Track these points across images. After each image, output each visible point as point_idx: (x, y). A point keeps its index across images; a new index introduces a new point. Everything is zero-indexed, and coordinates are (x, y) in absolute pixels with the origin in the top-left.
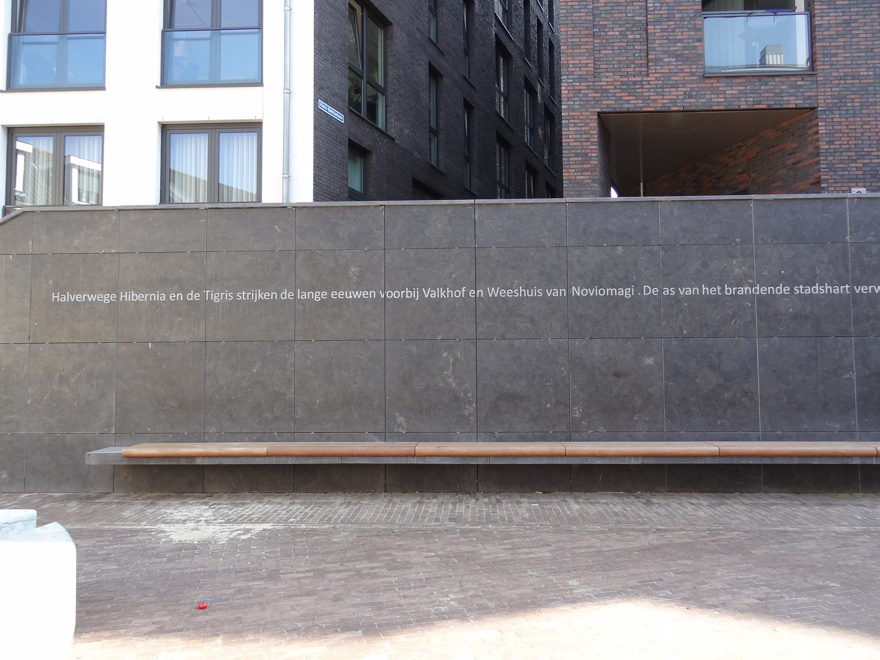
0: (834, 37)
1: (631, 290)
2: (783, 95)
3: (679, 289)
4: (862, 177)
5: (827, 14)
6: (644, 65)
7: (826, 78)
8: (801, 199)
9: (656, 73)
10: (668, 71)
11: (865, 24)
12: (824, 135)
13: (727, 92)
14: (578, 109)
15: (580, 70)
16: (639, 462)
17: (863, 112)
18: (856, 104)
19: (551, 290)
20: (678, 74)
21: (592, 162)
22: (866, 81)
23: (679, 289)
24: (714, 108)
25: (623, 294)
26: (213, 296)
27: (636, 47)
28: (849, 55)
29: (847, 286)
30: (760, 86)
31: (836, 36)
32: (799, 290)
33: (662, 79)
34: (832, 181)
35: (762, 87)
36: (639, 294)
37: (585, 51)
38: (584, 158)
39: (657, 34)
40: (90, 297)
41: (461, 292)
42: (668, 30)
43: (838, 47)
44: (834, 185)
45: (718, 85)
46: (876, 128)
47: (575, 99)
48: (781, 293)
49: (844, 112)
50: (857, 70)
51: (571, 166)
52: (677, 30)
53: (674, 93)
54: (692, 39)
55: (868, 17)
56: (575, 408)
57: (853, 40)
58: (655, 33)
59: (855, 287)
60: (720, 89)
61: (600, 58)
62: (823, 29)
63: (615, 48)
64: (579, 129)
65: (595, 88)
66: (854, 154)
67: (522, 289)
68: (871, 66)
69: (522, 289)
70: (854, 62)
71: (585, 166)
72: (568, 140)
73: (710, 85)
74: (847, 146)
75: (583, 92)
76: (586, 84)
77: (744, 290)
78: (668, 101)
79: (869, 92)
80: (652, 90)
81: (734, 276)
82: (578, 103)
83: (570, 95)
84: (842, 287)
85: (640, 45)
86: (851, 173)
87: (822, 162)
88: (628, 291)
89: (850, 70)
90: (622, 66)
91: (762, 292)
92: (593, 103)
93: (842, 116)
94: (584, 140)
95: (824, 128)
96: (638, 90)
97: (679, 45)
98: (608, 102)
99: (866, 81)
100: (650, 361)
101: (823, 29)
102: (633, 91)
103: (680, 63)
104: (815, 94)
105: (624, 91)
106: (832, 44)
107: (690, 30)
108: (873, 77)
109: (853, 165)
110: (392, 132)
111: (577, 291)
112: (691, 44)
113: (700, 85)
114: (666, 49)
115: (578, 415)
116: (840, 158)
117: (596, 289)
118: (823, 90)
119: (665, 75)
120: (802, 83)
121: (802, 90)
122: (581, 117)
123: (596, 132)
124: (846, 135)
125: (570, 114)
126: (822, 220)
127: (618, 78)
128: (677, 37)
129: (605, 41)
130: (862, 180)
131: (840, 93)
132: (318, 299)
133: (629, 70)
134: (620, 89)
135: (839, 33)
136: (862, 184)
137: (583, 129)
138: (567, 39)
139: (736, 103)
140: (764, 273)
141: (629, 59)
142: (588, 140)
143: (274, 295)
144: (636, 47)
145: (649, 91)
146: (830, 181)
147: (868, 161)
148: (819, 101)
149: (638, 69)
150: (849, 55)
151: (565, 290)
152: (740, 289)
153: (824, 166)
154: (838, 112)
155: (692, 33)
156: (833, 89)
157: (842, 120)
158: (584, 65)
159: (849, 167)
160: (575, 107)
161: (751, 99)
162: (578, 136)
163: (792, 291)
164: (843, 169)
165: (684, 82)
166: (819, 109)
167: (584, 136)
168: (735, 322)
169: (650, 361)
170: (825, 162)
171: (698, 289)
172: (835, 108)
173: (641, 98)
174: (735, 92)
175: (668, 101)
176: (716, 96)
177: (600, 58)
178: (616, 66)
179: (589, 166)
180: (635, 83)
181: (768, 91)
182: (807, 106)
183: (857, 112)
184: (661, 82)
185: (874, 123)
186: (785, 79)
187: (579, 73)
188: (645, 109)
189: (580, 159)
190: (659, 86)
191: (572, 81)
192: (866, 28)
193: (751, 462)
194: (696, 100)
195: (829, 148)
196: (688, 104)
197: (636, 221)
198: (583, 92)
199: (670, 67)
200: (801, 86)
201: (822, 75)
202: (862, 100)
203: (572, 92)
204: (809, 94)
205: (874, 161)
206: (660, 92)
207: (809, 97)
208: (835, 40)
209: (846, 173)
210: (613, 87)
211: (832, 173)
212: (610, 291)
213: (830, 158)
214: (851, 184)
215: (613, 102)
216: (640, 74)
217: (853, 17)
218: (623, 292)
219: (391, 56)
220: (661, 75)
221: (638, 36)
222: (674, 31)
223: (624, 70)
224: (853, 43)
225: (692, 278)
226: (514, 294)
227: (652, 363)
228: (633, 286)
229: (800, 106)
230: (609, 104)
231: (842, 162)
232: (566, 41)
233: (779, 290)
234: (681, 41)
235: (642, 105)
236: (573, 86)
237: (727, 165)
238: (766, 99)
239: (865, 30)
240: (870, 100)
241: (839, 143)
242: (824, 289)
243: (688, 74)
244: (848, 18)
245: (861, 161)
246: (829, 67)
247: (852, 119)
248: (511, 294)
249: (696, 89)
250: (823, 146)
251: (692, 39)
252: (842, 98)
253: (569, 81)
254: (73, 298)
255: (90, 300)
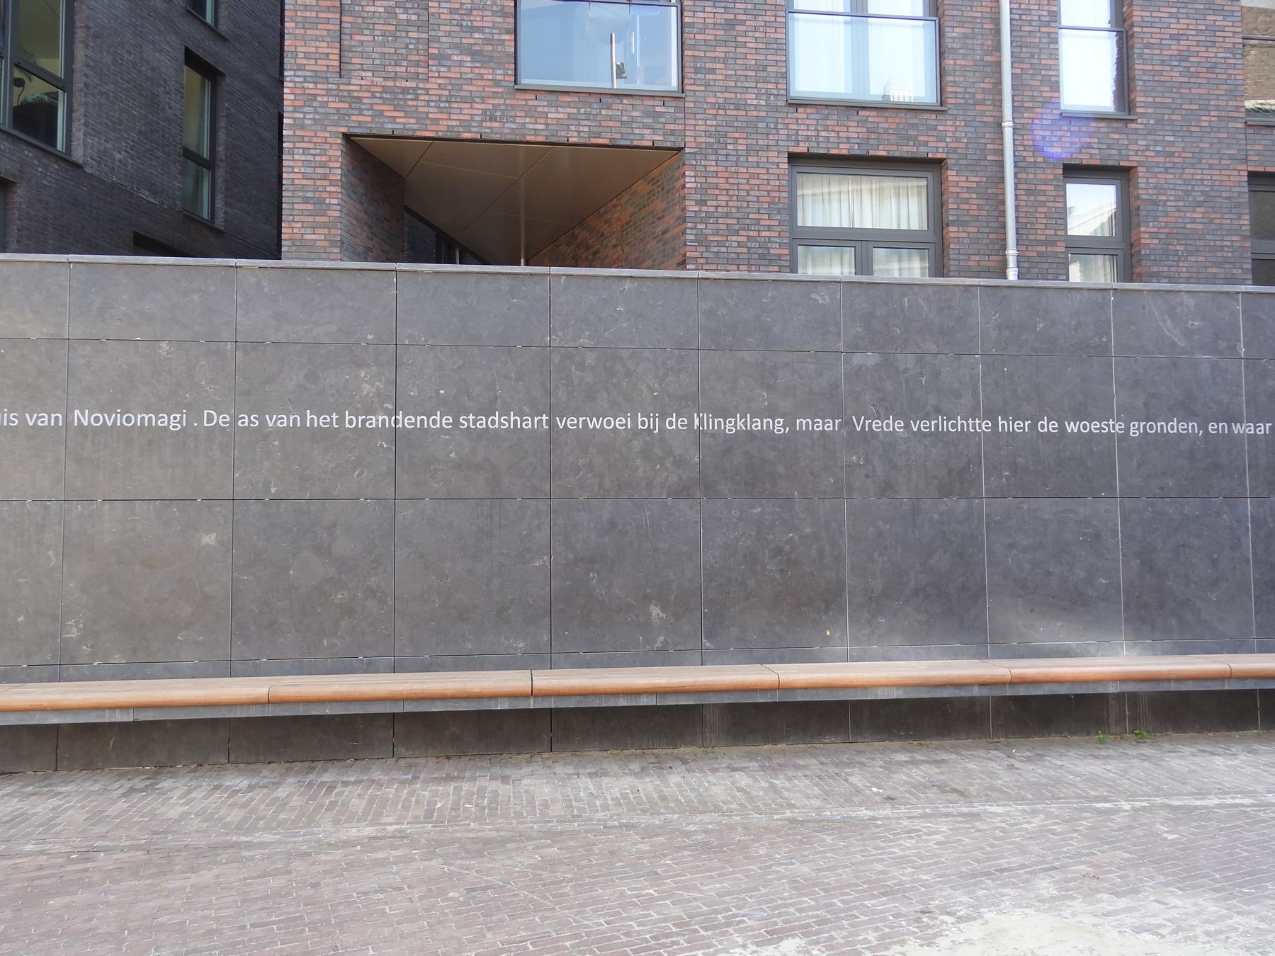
1: (181, 418)
2: (634, 125)
3: (267, 416)
5: (701, 9)
6: (422, 64)
8: (477, 273)
9: (439, 77)
10: (458, 76)
11: (756, 29)
12: (694, 191)
13: (549, 115)
14: (311, 125)
15: (316, 64)
16: (129, 717)
19: (36, 415)
20: (474, 82)
21: (330, 213)
22: (755, 113)
23: (267, 416)
24: (528, 138)
25: (166, 424)
27: (410, 34)
28: (733, 72)
29: (545, 418)
30: (600, 109)
31: (713, 43)
32: (467, 421)
33: (450, 87)
34: (703, 261)
35: (604, 112)
36: (196, 424)
37: (325, 33)
38: (318, 207)
39: (443, 16)
42: (461, 12)
45: (536, 103)
46: (768, 184)
47: (306, 109)
48: (438, 426)
49: (724, 158)
50: (743, 96)
51: (296, 218)
52: (474, 12)
53: (467, 111)
54: (498, 28)
55: (760, 18)
56: (70, 623)
57: (739, 50)
58: (439, 14)
59: (27, 415)
60: (540, 109)
61: (352, 46)
62: (695, 30)
63: (377, 33)
64: (310, 158)
65: (341, 94)
66: (735, 221)
68: (763, 91)
70: (739, 84)
71: (318, 219)
72: (291, 176)
73: (524, 103)
74: (725, 209)
75: (319, 99)
76: (325, 86)
77: (377, 420)
78: (458, 123)
80: (432, 104)
81: (360, 396)
82: (311, 116)
83: (297, 103)
84: (536, 419)
85: (418, 32)
86: (730, 250)
87: (688, 231)
88: (175, 418)
89: (733, 96)
90: (387, 63)
91: (406, 425)
92: (336, 117)
93: (719, 163)
94: (319, 176)
95: (693, 179)
96: (410, 103)
97: (476, 35)
98: (361, 118)
99: (755, 113)
100: (209, 539)
101: (695, 30)
102: (402, 103)
103: (478, 65)
104: (681, 127)
105: (387, 102)
106: (708, 54)
107: (494, 13)
108: (765, 108)
109: (734, 238)
110: (78, 155)
111: (82, 417)
112: (496, 37)
113: (508, 102)
114: (457, 40)
115: (74, 634)
116: (715, 226)
117: (119, 415)
119: (453, 81)
120: (663, 109)
122: (315, 140)
123: (338, 165)
124: (725, 192)
125: (297, 134)
126: (508, 309)
127: (379, 81)
128: (475, 24)
129: (360, 20)
130: (746, 262)
131: (718, 128)
132: (1135, 433)
133: (398, 69)
134: (380, 98)
135: (718, 38)
137: (318, 158)
138: (296, 11)
139: (563, 134)
140: (412, 393)
141: (398, 52)
142: (324, 177)
144: (410, 34)
145: (428, 106)
147: (755, 234)
149: (412, 70)
151: (60, 416)
152: (371, 419)
153: (692, 237)
154: (713, 157)
155: (498, 20)
157: (720, 169)
158: (322, 56)
160: (306, 122)
161: (586, 129)
162: (309, 170)
163: (456, 423)
165: (483, 95)
166: (687, 150)
167: (318, 170)
168: (359, 475)
169: (209, 539)
170: (694, 232)
171: (298, 418)
172: (710, 151)
173: (414, 115)
174: (561, 116)
175: (458, 123)
176: (532, 120)
177: (352, 46)
178: (377, 62)
179: (325, 219)
180: (405, 91)
181: (611, 118)
182: (669, 145)
183: (742, 159)
184: (446, 93)
185: (766, 177)
186: (637, 102)
187: (314, 68)
188: (419, 134)
189: (310, 207)
190: (444, 99)
191: (302, 79)
192: (757, 34)
193: (328, 712)
194: (501, 125)
195: (700, 211)
196: (489, 131)
197: (196, 299)
198: (319, 99)
199: (463, 70)
200: (661, 114)
201: (692, 99)
203: (301, 97)
204: (672, 127)
205: (764, 234)
206: (445, 107)
207: (673, 132)
208: (712, 49)
209: (723, 249)
210: (368, 95)
211: (703, 249)
212: (143, 419)
213: (699, 226)
215: (369, 119)
216: (416, 77)
217: (739, 17)
218: (166, 420)
219: (81, 27)
220: (447, 81)
221: (414, 17)
222: (470, 14)
223: (390, 69)
224: (738, 56)
225: (290, 399)
226: (1101, 428)
227: (214, 543)
228: (185, 411)
229: (660, 145)
230: (361, 122)
231: (717, 232)
232: (294, 14)
233: (435, 422)
234: (480, 30)
235: (416, 126)
236: (303, 87)
237: (602, 234)
238: (608, 130)
240: (761, 142)
241: (714, 203)
242: (509, 421)
243: (491, 83)
244: (732, 17)
246: (703, 88)
247: (733, 169)
249: (503, 107)
250: (692, 207)
251: (498, 28)
252: (721, 137)
253: (297, 79)
254: (271, 421)
255: (591, 427)
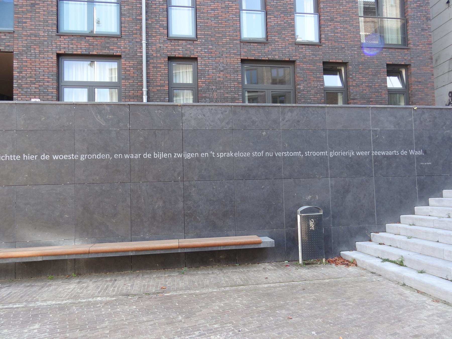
0: (25, 12)
4: (38, 93)
7: (19, 35)
11: (44, 6)
12: (17, 68)
17: (41, 56)
18: (36, 51)
22: (43, 38)
26: (187, 155)
28: (34, 23)
40: (54, 157)
41: (261, 154)
43: (27, 18)
44: (21, 97)
50: (38, 32)
57: (36, 15)
67: (25, 155)
68: (46, 30)
69: (25, 155)
70: (36, 27)
74: (30, 75)
79: (44, 45)
84: (393, 152)
86: (32, 90)
95: (17, 64)
99: (43, 38)
104: (12, 44)
106: (24, 16)
108: (47, 37)
109: (33, 86)
118: (17, 42)
120: (5, 37)
121: (4, 41)
124: (30, 68)
131: (28, 44)
135: (28, 10)
136: (38, 97)
143: (170, 155)
146: (19, 94)
147: (42, 84)
148: (14, 48)
150: (34, 23)
154: (25, 55)
156: (23, 42)
157: (28, 60)
159: (31, 87)
164: (27, 88)
166: (14, 53)
172: (24, 53)
182: (7, 51)
192: (44, 9)
195: (20, 76)
201: (17, 33)
202: (40, 49)
204: (8, 44)
205: (46, 84)
207: (8, 46)
208: (26, 14)
209: (29, 90)
211: (20, 90)
212: (295, 153)
213: (19, 81)
214: (31, 97)
224: (36, 17)
226: (68, 157)
239: (44, 10)
240: (45, 49)
241: (25, 73)
245: (38, 84)
246: (21, 29)
248: (66, 158)
252: (28, 48)
